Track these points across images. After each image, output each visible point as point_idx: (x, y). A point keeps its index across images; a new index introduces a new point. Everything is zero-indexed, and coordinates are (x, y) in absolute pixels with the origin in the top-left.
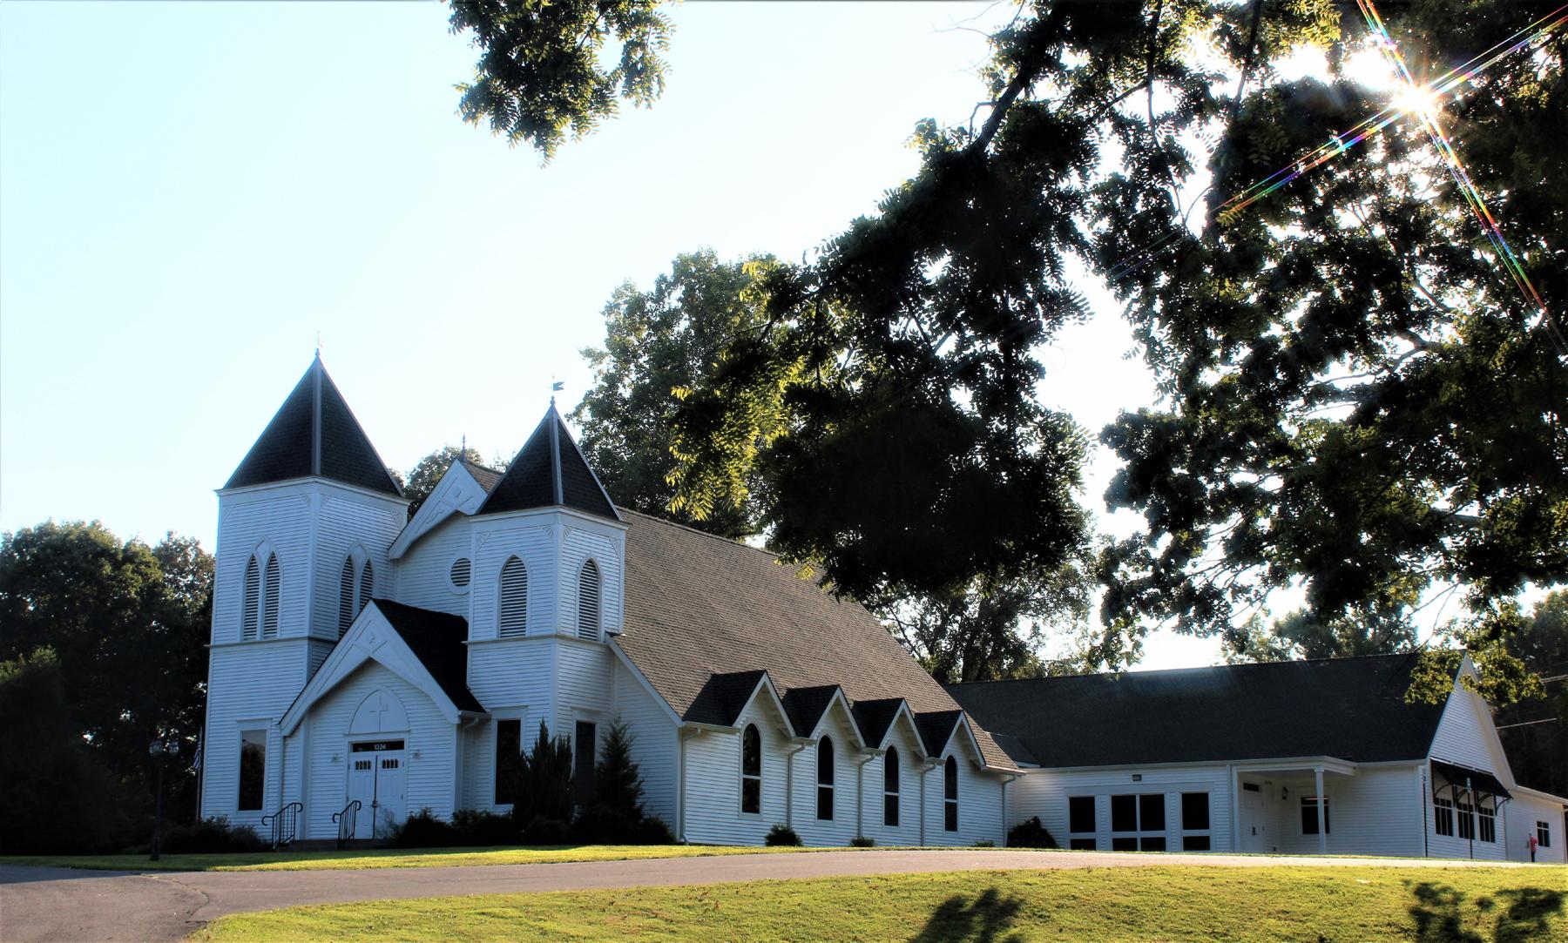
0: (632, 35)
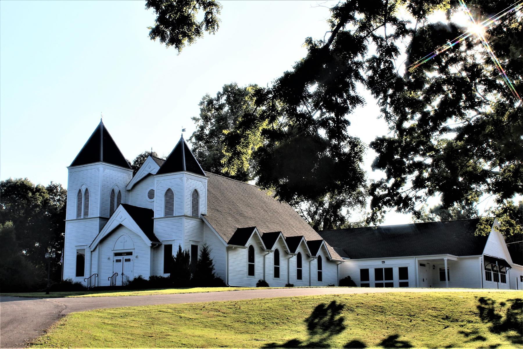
0: (208, 10)
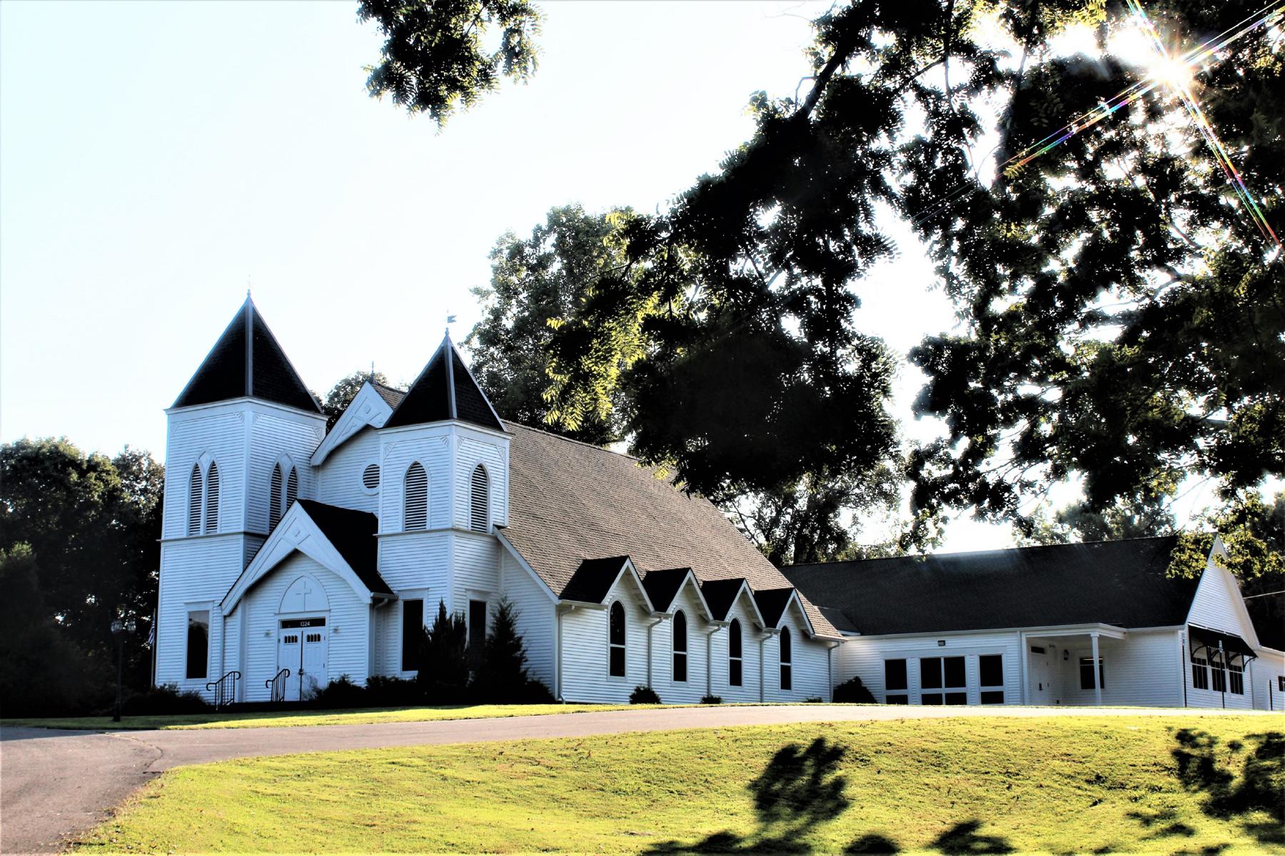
0: (511, 23)
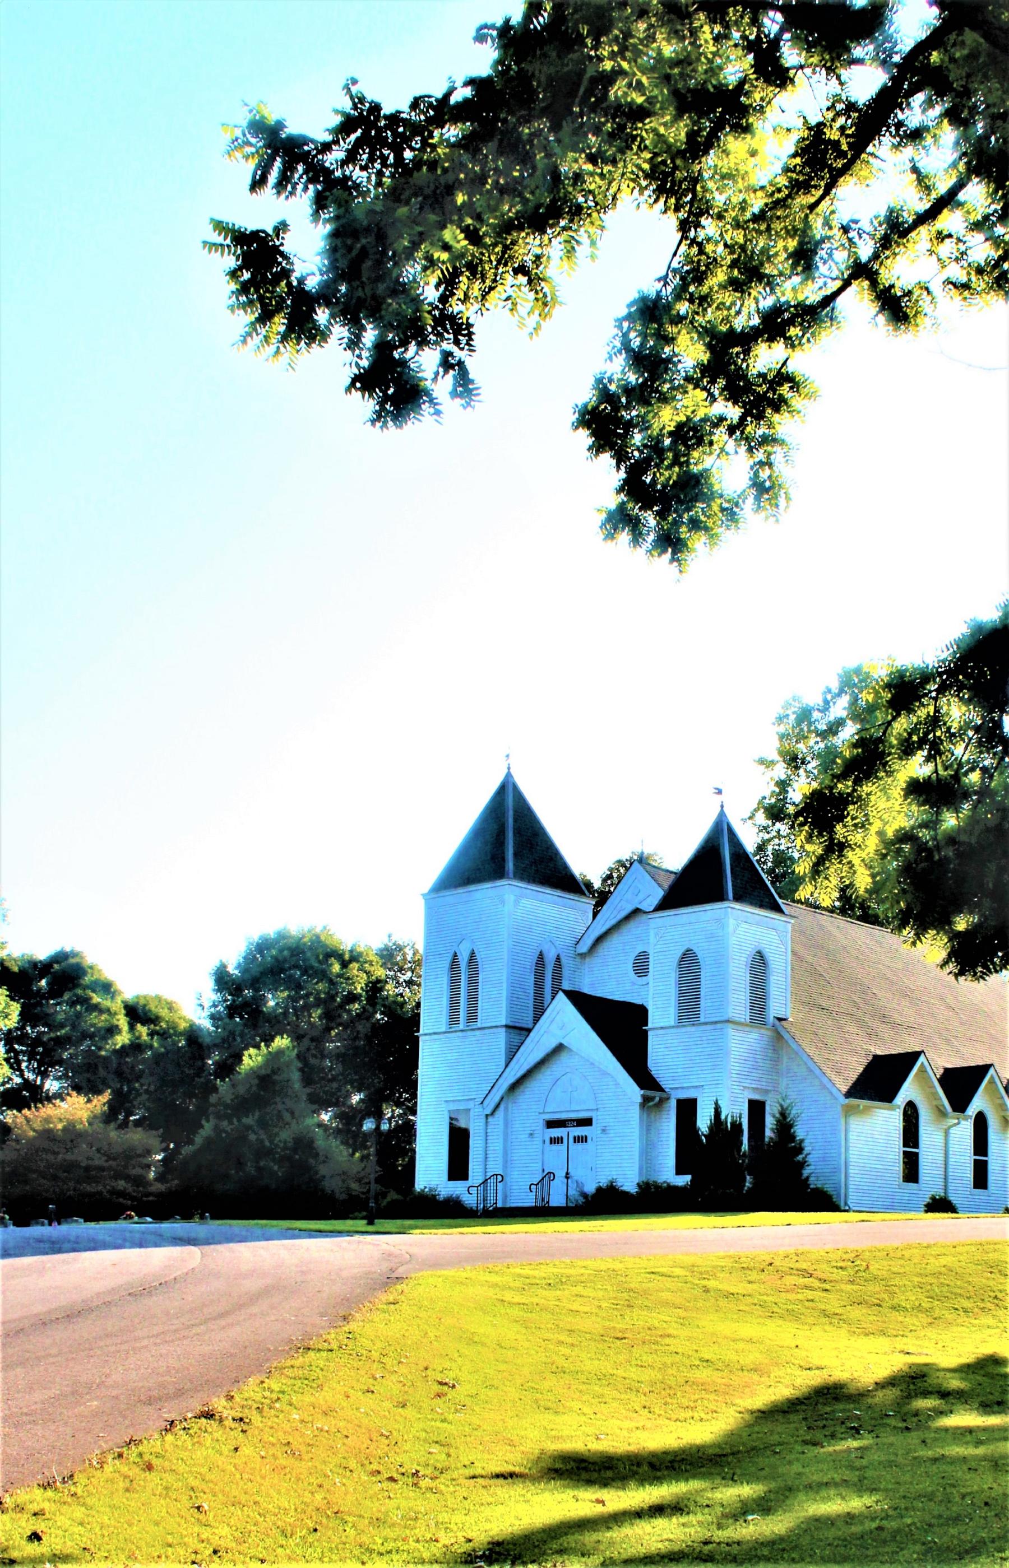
0: (760, 455)
